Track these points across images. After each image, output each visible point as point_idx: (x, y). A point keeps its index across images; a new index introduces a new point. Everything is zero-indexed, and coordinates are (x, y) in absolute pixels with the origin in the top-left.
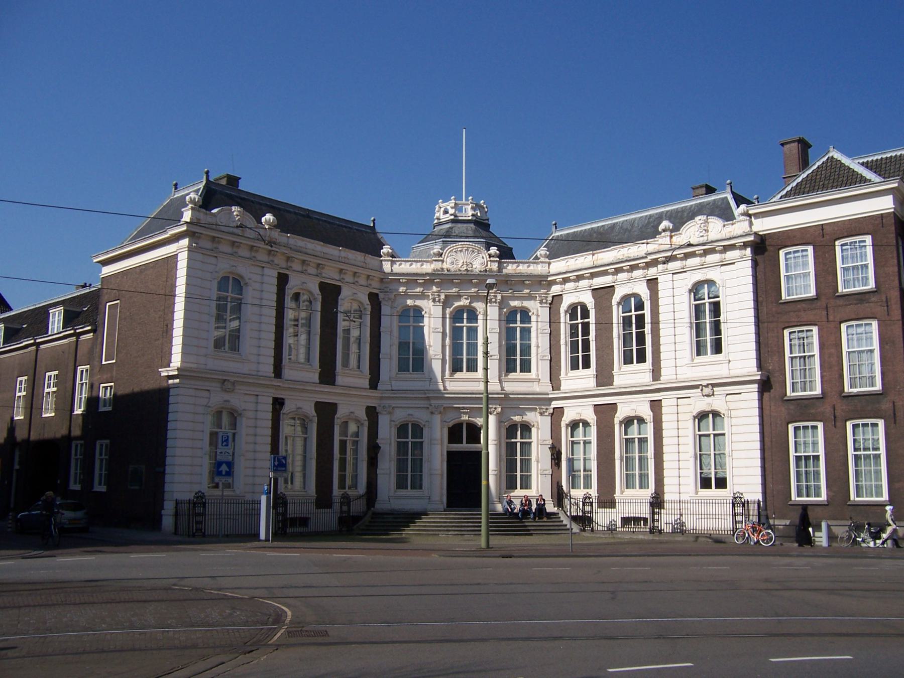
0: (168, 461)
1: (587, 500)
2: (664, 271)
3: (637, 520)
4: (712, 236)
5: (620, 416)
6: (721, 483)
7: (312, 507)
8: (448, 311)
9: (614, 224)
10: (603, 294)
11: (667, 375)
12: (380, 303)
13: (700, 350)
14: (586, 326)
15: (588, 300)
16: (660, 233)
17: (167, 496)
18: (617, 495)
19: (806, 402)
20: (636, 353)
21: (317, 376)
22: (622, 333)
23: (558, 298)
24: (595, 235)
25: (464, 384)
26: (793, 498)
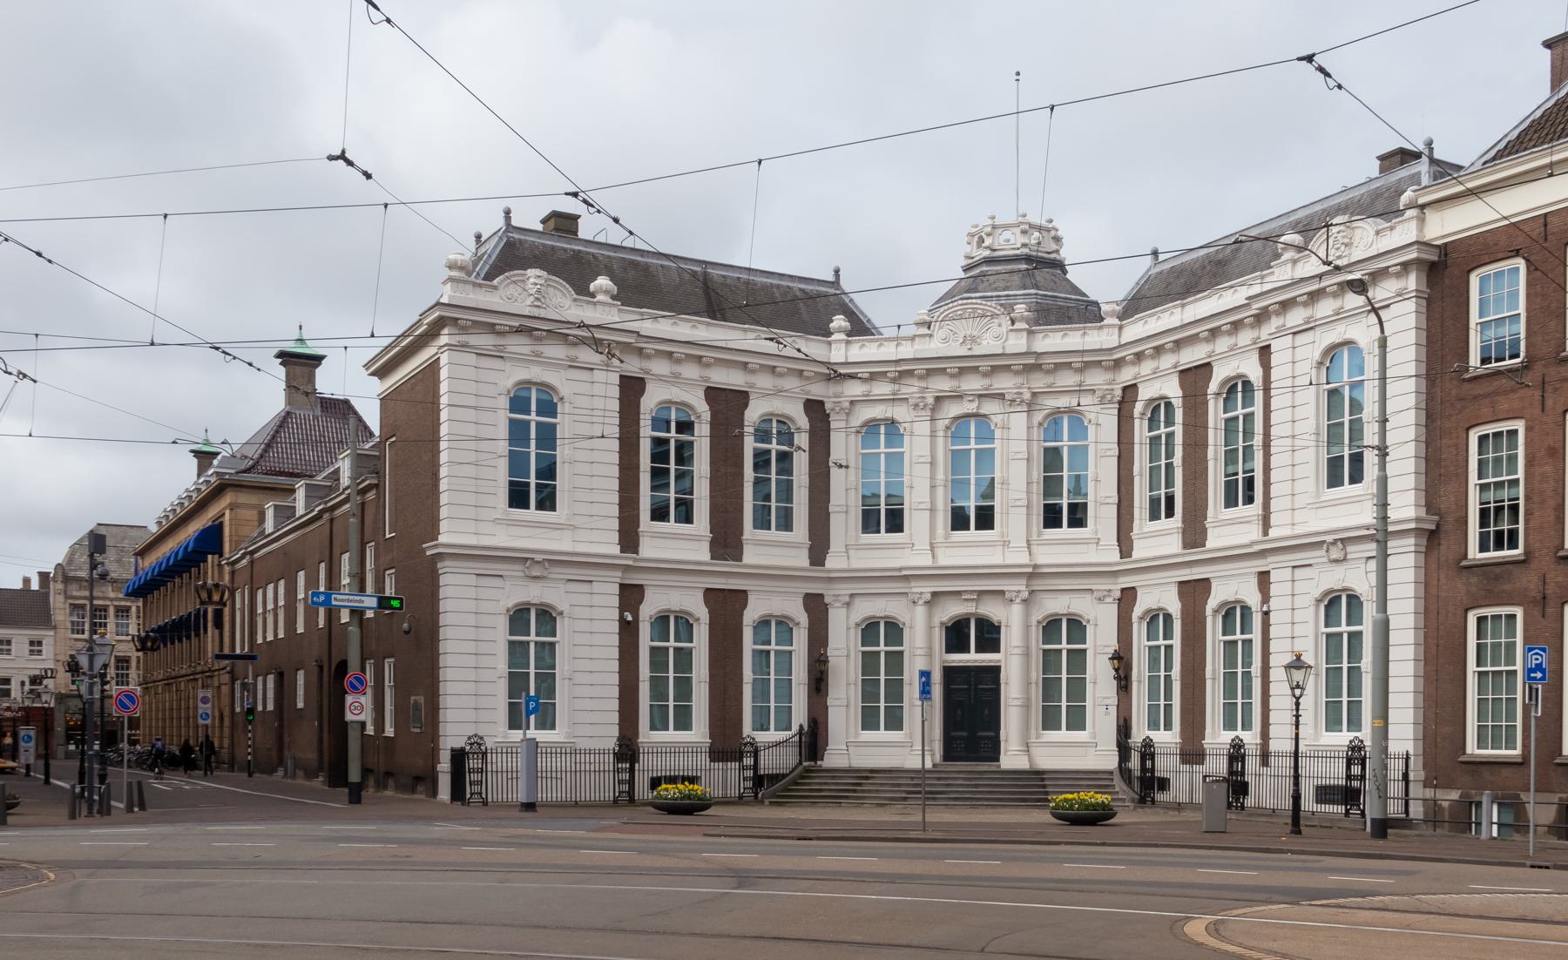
2: (1280, 332)
7: (704, 760)
8: (941, 424)
15: (1172, 389)
19: (1497, 570)
20: (1241, 491)
21: (706, 546)
26: (1469, 750)
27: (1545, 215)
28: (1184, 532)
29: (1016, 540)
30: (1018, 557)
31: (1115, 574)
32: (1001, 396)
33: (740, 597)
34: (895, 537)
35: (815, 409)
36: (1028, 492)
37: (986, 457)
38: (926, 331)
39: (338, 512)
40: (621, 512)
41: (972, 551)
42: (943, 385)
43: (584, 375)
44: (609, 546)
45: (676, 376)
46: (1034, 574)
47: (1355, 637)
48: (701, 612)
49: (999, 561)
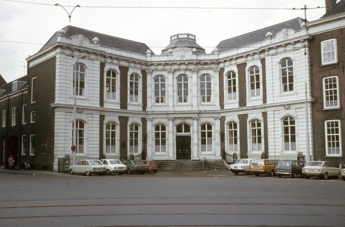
1: (235, 156)
2: (268, 55)
10: (242, 67)
11: (269, 101)
14: (234, 81)
15: (235, 69)
18: (248, 154)
21: (119, 105)
22: (250, 83)
23: (222, 70)
25: (160, 108)
27: (341, 29)
30: (195, 109)
31: (219, 113)
32: (190, 70)
33: (127, 118)
34: (292, 92)
35: (144, 72)
36: (197, 93)
37: (163, 86)
39: (11, 97)
42: (175, 67)
44: (97, 105)
46: (200, 113)
47: (236, 132)
49: (190, 110)
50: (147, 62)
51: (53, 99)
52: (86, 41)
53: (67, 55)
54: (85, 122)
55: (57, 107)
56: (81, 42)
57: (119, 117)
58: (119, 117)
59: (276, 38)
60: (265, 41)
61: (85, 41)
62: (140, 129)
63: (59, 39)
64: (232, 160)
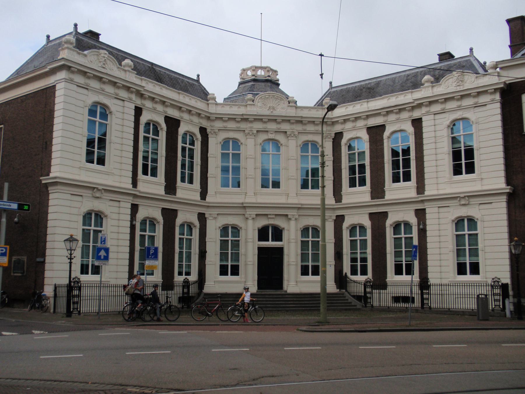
0: (48, 252)
2: (428, 113)
3: (405, 299)
4: (467, 86)
5: (390, 222)
6: (475, 269)
9: (379, 81)
11: (430, 191)
12: (208, 135)
13: (457, 171)
16: (423, 85)
17: (46, 281)
21: (163, 188)
24: (364, 90)
28: (371, 193)
29: (291, 193)
30: (293, 200)
35: (203, 131)
38: (252, 103)
40: (422, 142)
41: (271, 197)
43: (120, 103)
45: (155, 109)
48: (160, 218)
50: (211, 113)
51: (46, 169)
52: (111, 64)
53: (78, 86)
54: (106, 216)
55: (55, 184)
56: (104, 64)
57: (163, 209)
58: (163, 209)
59: (442, 86)
60: (421, 90)
61: (111, 63)
62: (196, 233)
63: (64, 54)
64: (363, 292)
